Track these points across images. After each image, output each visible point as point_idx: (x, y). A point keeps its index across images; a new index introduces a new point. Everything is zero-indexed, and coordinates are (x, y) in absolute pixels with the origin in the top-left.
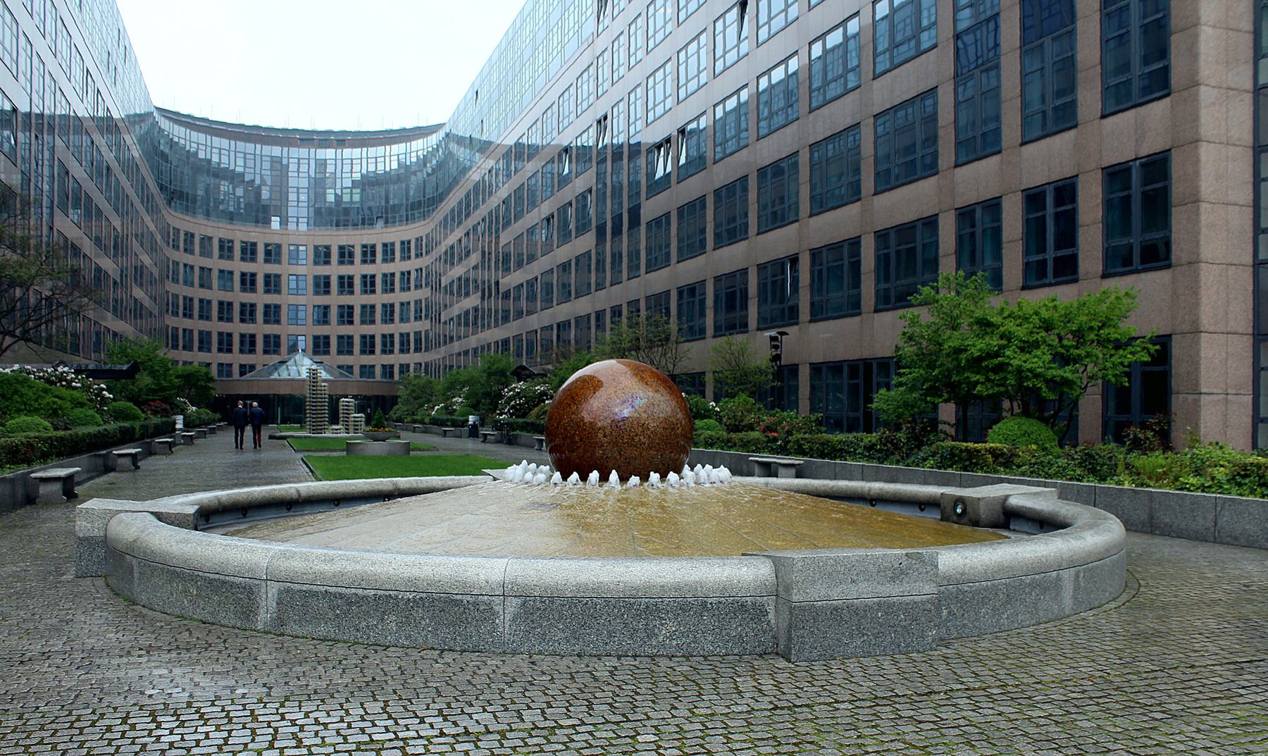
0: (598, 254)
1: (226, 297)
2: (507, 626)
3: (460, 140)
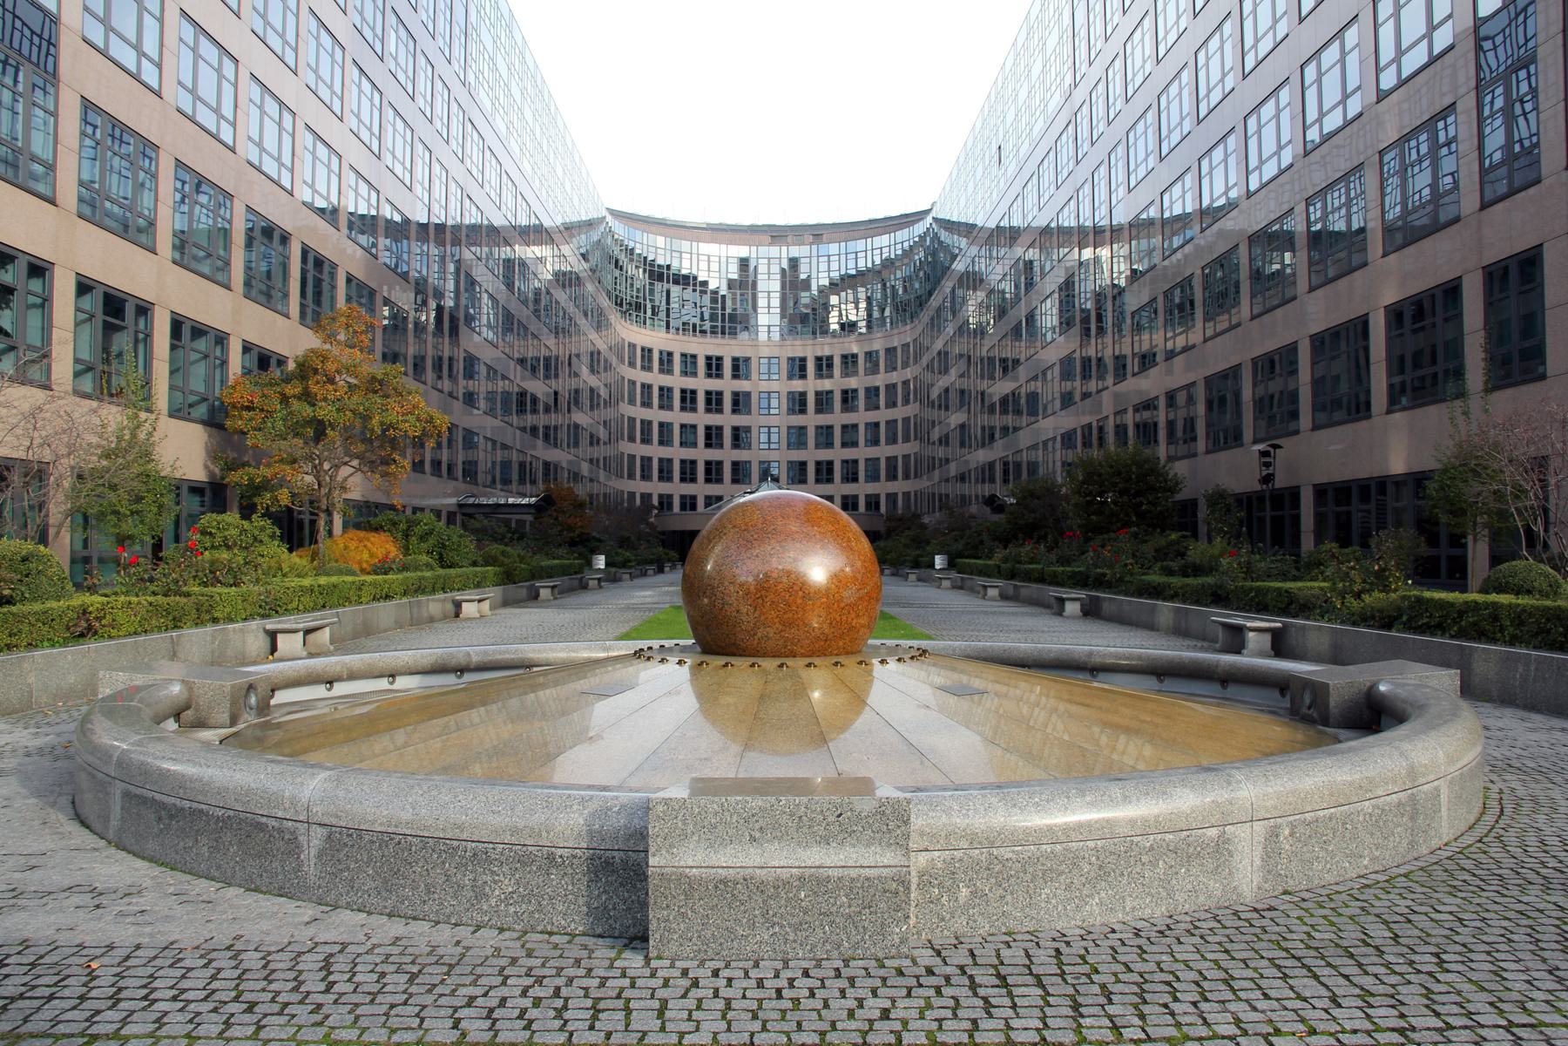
3: (948, 225)
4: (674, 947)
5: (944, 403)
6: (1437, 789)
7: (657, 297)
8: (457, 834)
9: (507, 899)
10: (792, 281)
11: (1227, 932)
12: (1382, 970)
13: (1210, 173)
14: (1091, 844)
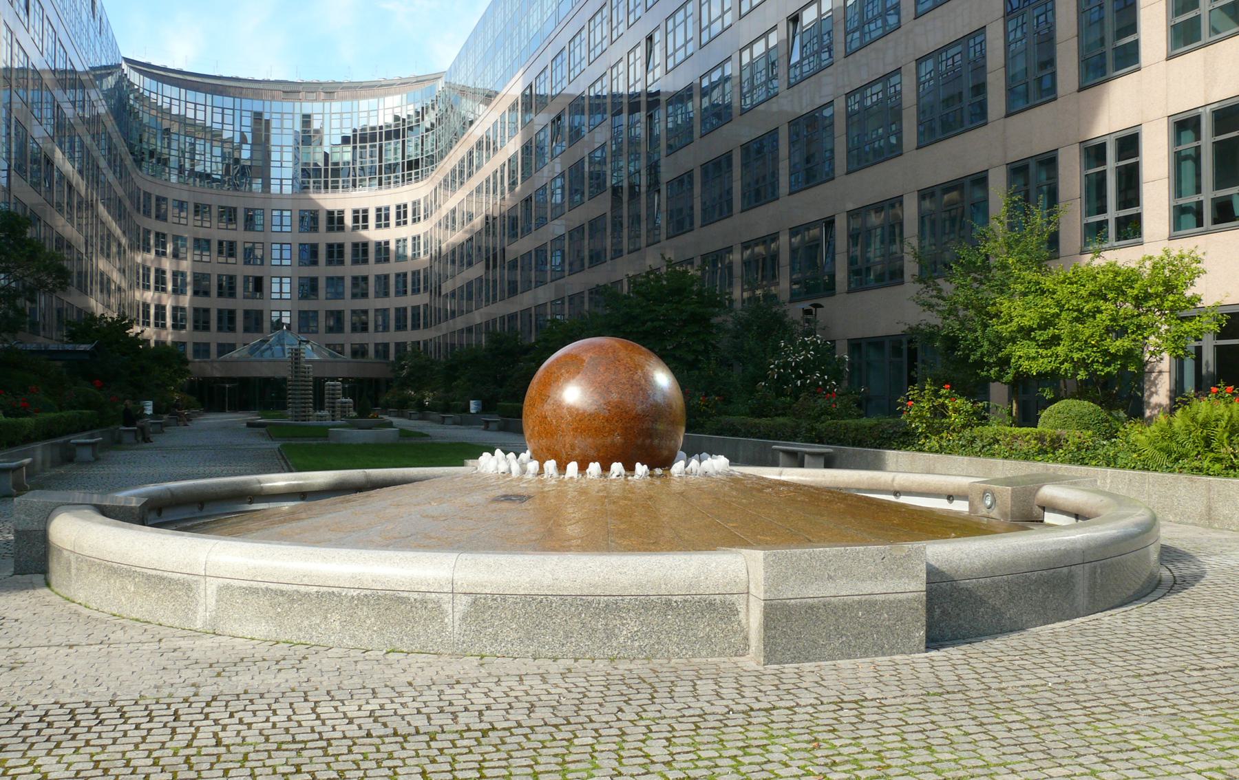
0: (613, 217)
2: (456, 625)
8: (592, 591)
13: (674, 30)
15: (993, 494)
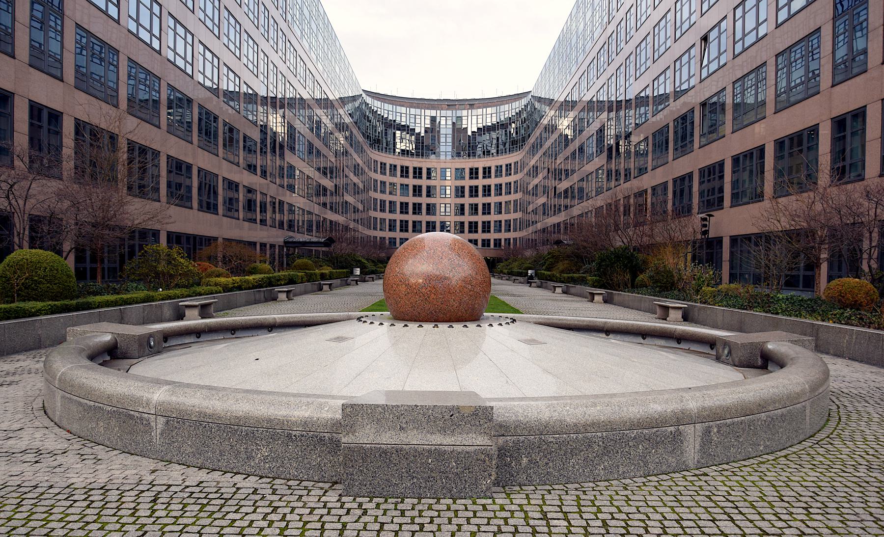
1: (404, 199)
3: (540, 99)
4: (356, 489)
5: (535, 192)
6: (804, 407)
7: (389, 136)
9: (265, 459)
10: (458, 130)
11: (679, 488)
12: (774, 518)
13: (681, 69)
14: (599, 434)
15: (729, 347)
